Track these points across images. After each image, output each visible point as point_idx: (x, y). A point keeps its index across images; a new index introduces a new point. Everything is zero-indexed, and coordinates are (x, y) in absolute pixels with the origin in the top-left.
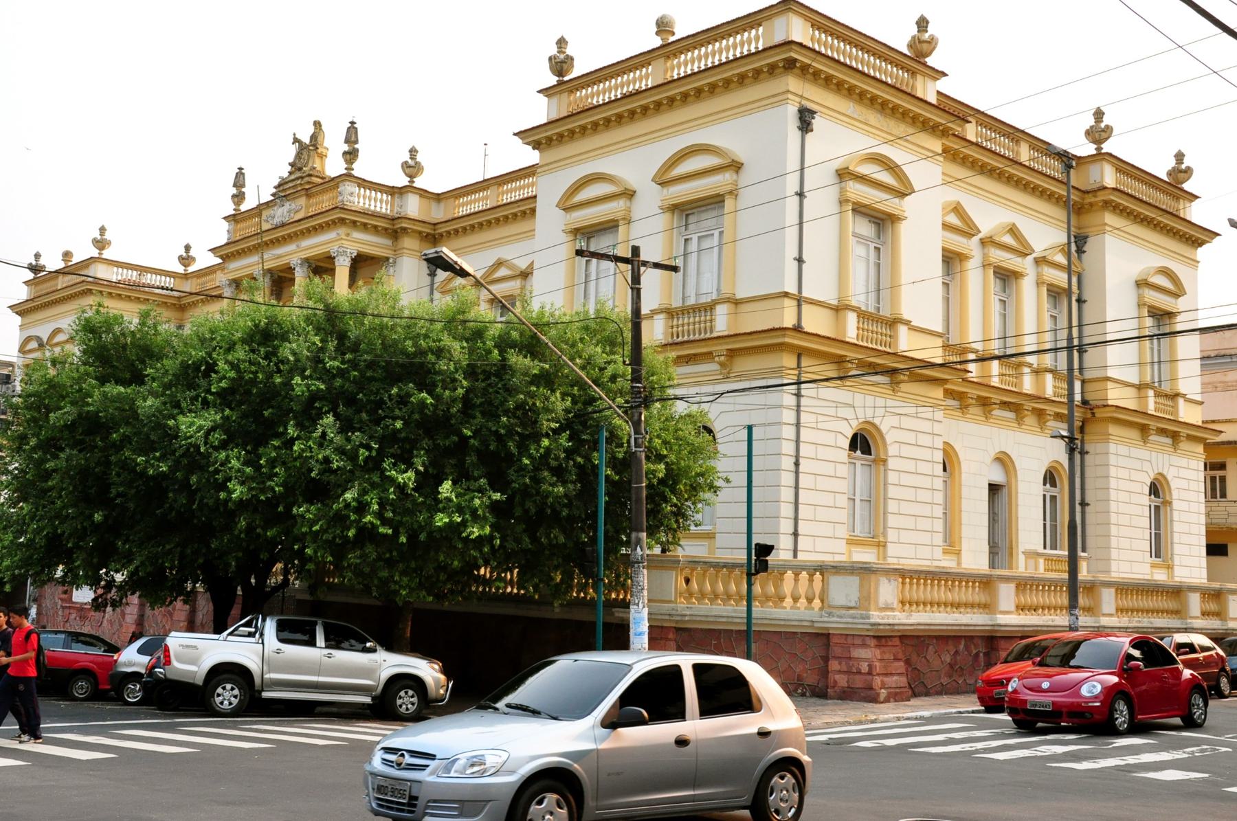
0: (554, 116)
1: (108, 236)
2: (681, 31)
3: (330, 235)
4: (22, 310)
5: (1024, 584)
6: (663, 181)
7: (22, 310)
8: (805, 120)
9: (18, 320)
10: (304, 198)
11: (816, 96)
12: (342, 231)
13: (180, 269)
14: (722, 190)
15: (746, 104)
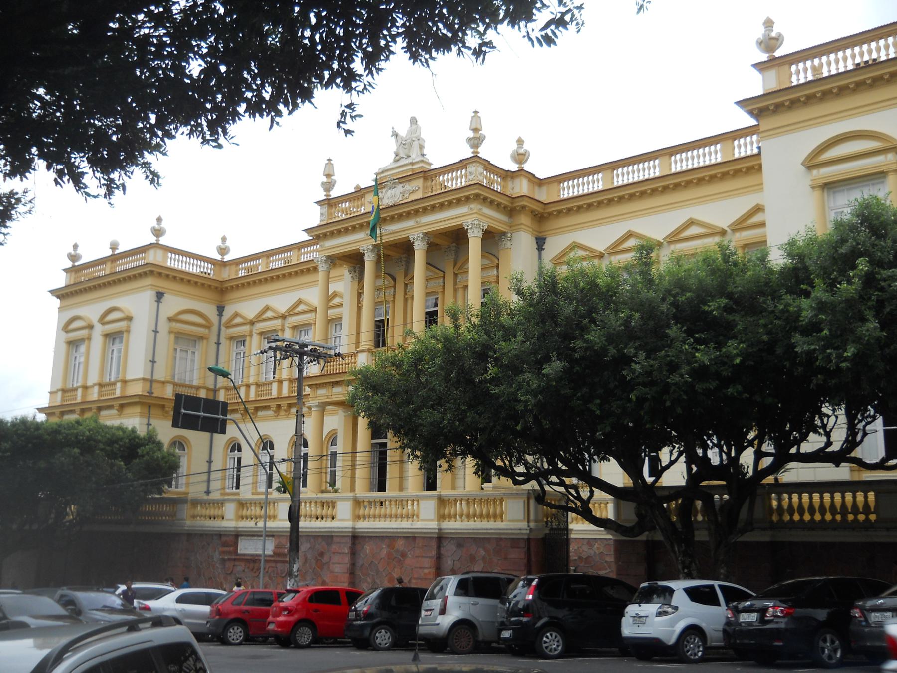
0: (68, 283)
1: (164, 225)
2: (121, 249)
3: (463, 210)
4: (61, 294)
5: (242, 504)
6: (102, 320)
7: (61, 294)
8: (160, 296)
9: (57, 302)
10: (421, 180)
11: (163, 284)
12: (475, 206)
13: (219, 257)
14: (884, 169)
15: (869, 105)
